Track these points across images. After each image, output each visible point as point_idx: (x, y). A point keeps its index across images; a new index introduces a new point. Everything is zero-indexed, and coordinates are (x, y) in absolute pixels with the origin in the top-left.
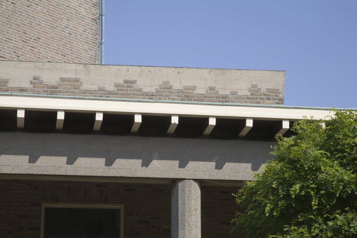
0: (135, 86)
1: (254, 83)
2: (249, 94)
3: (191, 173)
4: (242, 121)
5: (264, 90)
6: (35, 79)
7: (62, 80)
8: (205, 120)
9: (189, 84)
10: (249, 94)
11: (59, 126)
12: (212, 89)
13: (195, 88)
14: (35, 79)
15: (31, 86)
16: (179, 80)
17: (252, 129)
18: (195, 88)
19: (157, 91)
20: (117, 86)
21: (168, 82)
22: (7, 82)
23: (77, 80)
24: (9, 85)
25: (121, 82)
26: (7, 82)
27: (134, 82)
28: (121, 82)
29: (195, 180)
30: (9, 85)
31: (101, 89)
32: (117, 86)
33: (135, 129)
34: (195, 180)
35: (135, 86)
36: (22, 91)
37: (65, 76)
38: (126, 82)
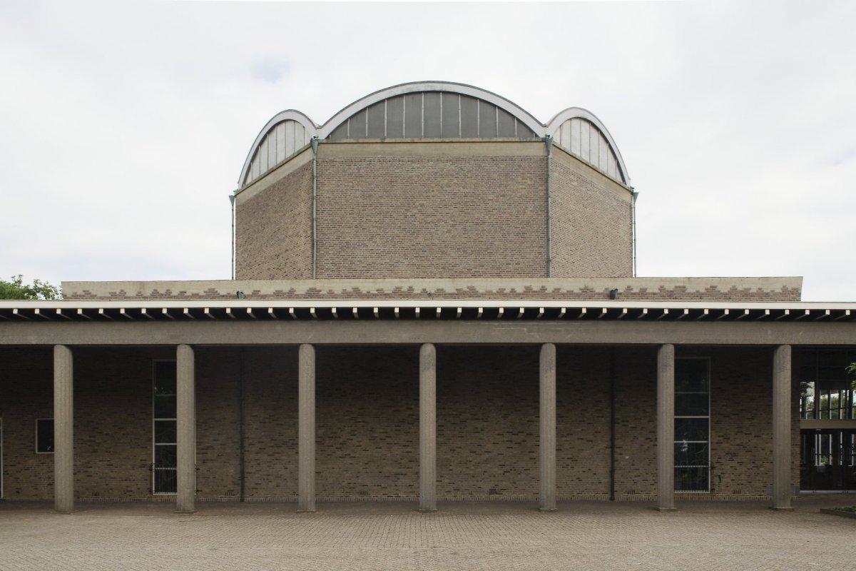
0: (716, 290)
1: (785, 284)
2: (781, 291)
3: (306, 338)
4: (601, 309)
5: (790, 289)
6: (661, 287)
7: (676, 287)
8: (559, 309)
9: (747, 287)
10: (781, 291)
11: (438, 316)
12: (760, 289)
13: (750, 289)
14: (661, 287)
15: (580, 292)
16: (419, 285)
17: (544, 314)
18: (750, 289)
19: (253, 293)
20: (706, 289)
21: (735, 286)
22: (646, 289)
23: (684, 287)
24: (647, 291)
25: (709, 287)
26: (646, 289)
27: (716, 287)
28: (709, 287)
29: (553, 343)
30: (647, 291)
31: (197, 294)
32: (706, 289)
33: (479, 316)
34: (553, 343)
35: (716, 290)
36: (102, 299)
37: (678, 285)
38: (711, 287)
